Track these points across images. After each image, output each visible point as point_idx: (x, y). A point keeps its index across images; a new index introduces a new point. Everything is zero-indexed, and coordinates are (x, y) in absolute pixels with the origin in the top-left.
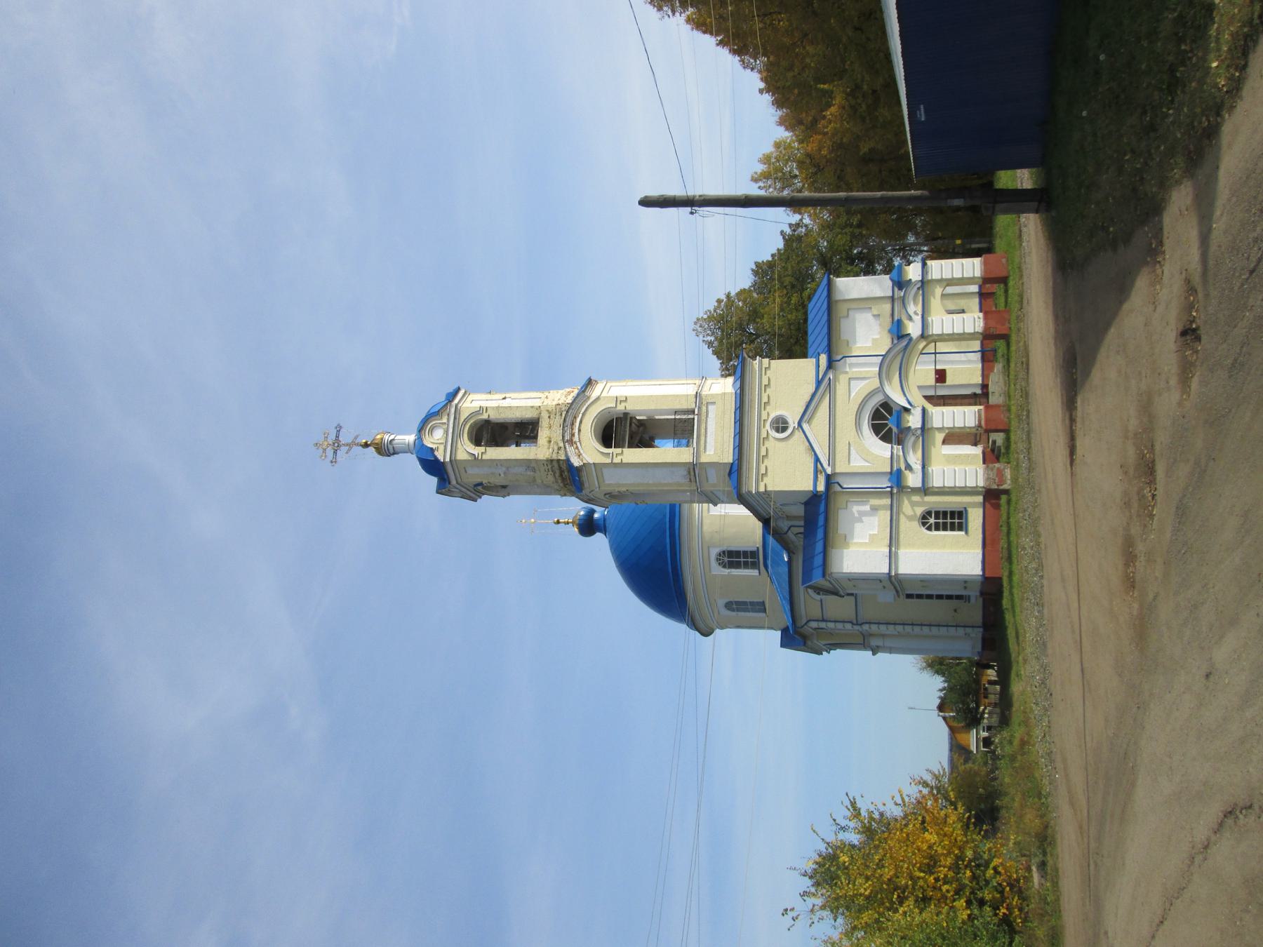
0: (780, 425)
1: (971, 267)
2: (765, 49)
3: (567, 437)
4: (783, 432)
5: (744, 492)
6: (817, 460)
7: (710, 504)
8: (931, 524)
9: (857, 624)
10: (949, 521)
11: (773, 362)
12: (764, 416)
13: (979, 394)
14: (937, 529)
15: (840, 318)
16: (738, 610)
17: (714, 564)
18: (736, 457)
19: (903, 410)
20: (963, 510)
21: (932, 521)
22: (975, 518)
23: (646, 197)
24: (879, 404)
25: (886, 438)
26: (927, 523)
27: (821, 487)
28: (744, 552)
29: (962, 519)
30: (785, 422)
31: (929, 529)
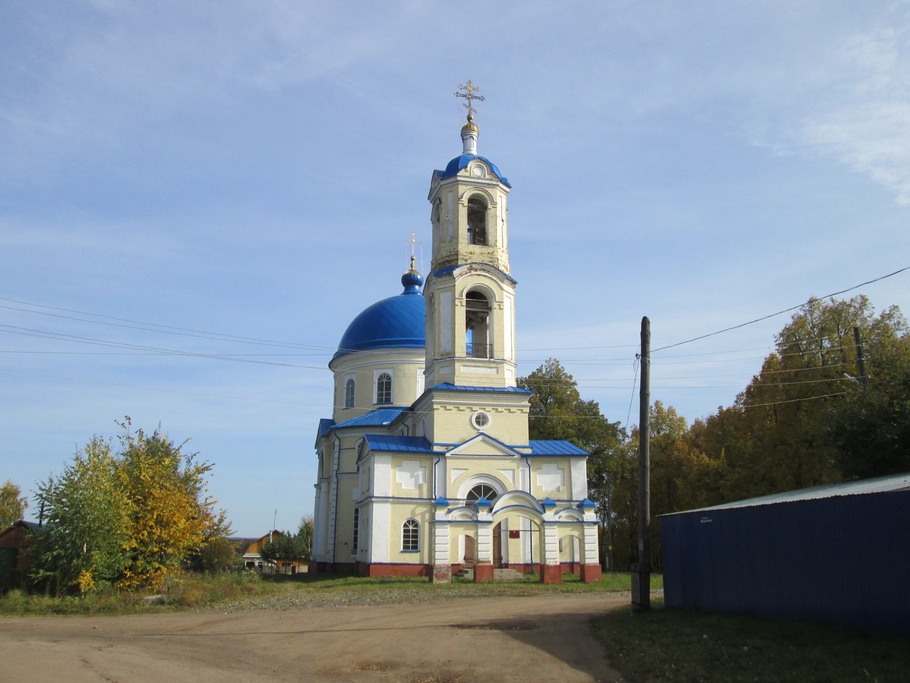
0: (481, 420)
1: (592, 557)
5: (434, 393)
6: (456, 446)
8: (408, 527)
12: (488, 408)
18: (459, 388)
19: (490, 507)
21: (411, 528)
22: (412, 558)
24: (495, 491)
27: (436, 449)
30: (483, 424)
31: (405, 525)
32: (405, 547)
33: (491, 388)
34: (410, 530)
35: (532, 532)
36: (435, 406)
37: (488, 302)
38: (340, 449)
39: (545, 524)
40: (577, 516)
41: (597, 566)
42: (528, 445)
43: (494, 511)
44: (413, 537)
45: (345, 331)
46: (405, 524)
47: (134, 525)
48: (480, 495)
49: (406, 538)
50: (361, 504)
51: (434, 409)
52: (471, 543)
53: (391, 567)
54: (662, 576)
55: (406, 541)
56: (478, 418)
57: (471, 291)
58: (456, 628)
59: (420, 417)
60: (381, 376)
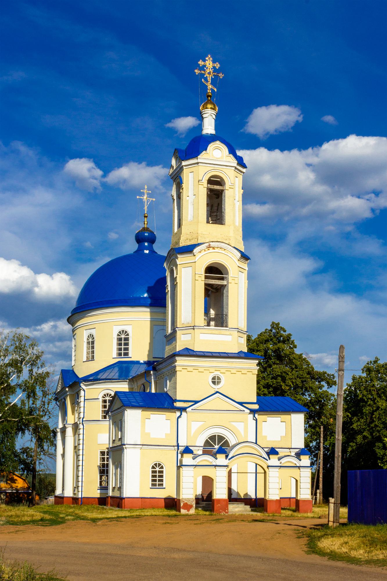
0: (216, 381)
1: (305, 494)
2: (5, 503)
3: (212, 244)
4: (221, 438)
5: (176, 358)
6: (196, 402)
7: (253, 497)
8: (155, 468)
9: (83, 421)
10: (157, 479)
11: (256, 376)
12: (223, 370)
13: (231, 496)
14: (153, 472)
15: (290, 415)
16: (88, 343)
17: (121, 328)
18: (198, 353)
19: (227, 454)
20: (164, 487)
21: (158, 469)
22: (160, 494)
23: (169, 496)
24: (228, 440)
25: (207, 443)
26: (156, 467)
27: (178, 404)
28: (128, 343)
29: (158, 486)
30: (219, 383)
31: (153, 467)
32: (153, 485)
33: (225, 353)
34: (157, 471)
35: (175, 444)
36: (178, 369)
37: (223, 287)
38: (85, 400)
39: (269, 468)
40: (295, 462)
41: (309, 501)
42: (255, 401)
43: (230, 457)
44: (155, 476)
45: (85, 283)
46: (153, 466)
47: (368, 437)
48: (218, 445)
49: (153, 477)
50: (143, 447)
51: (176, 371)
52: (208, 482)
53: (140, 499)
54: (146, 432)
55: (162, 477)
56: (214, 378)
57: (209, 266)
58: (181, 191)
59: (162, 375)
60: (120, 332)
